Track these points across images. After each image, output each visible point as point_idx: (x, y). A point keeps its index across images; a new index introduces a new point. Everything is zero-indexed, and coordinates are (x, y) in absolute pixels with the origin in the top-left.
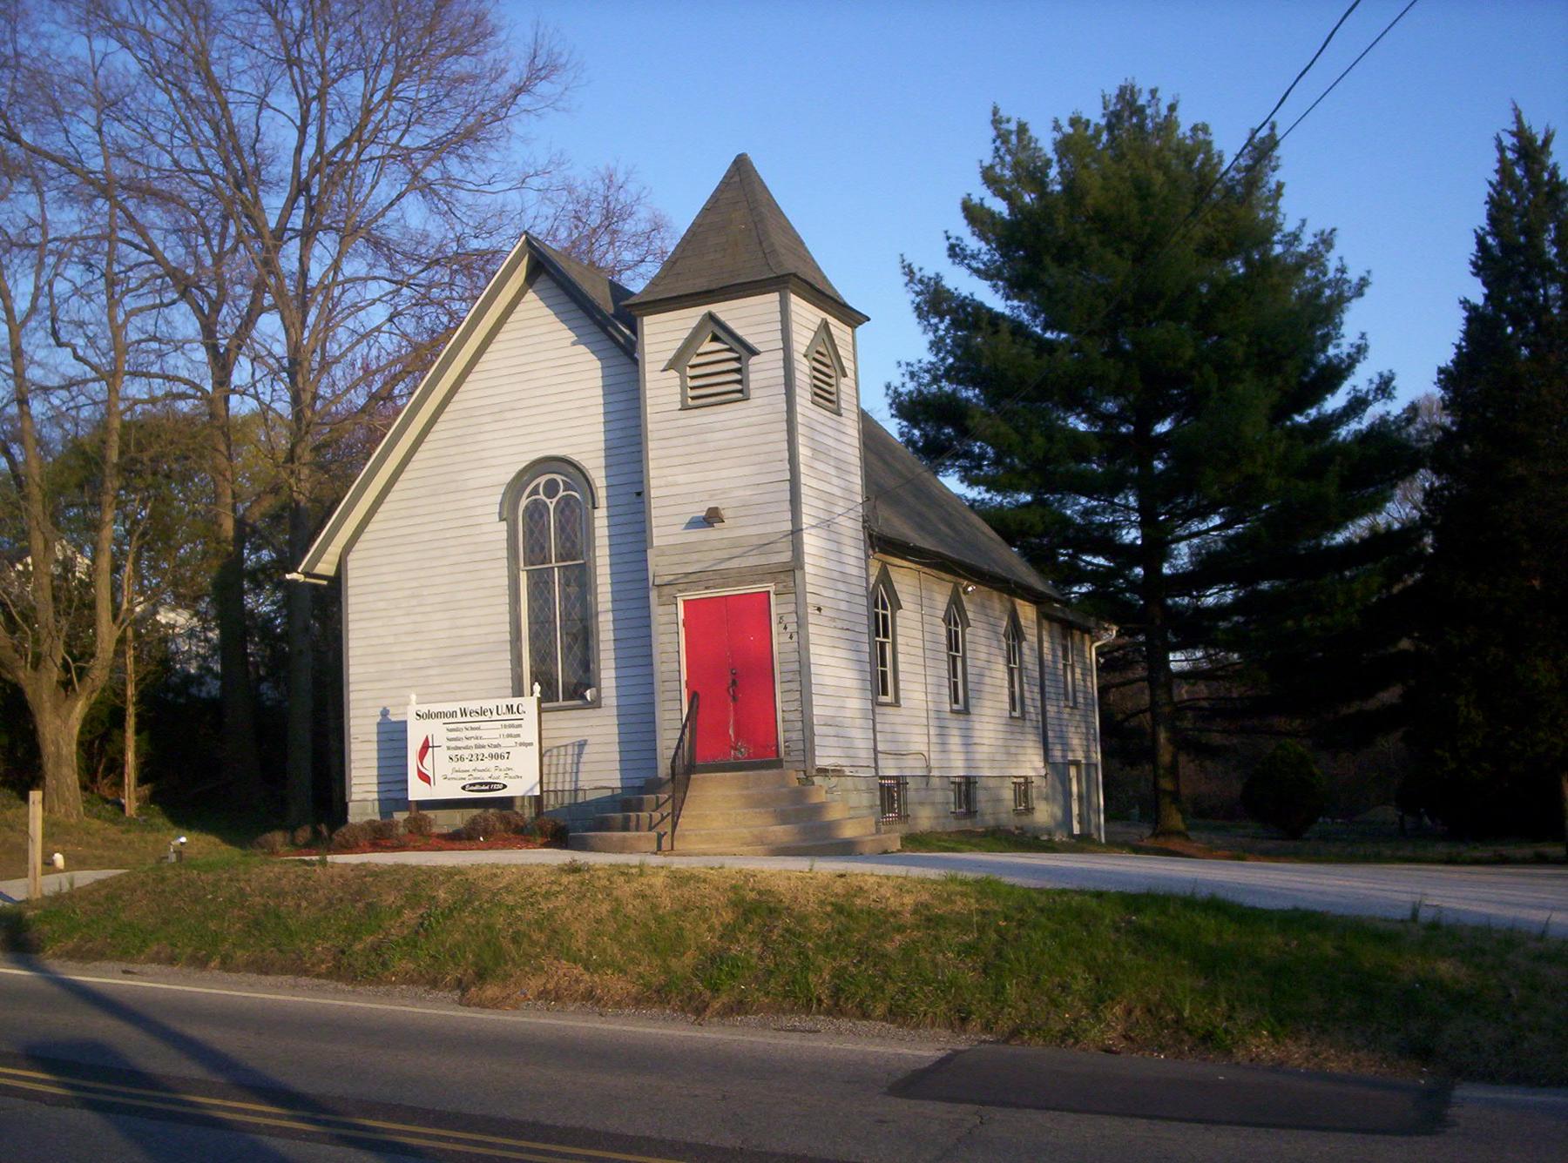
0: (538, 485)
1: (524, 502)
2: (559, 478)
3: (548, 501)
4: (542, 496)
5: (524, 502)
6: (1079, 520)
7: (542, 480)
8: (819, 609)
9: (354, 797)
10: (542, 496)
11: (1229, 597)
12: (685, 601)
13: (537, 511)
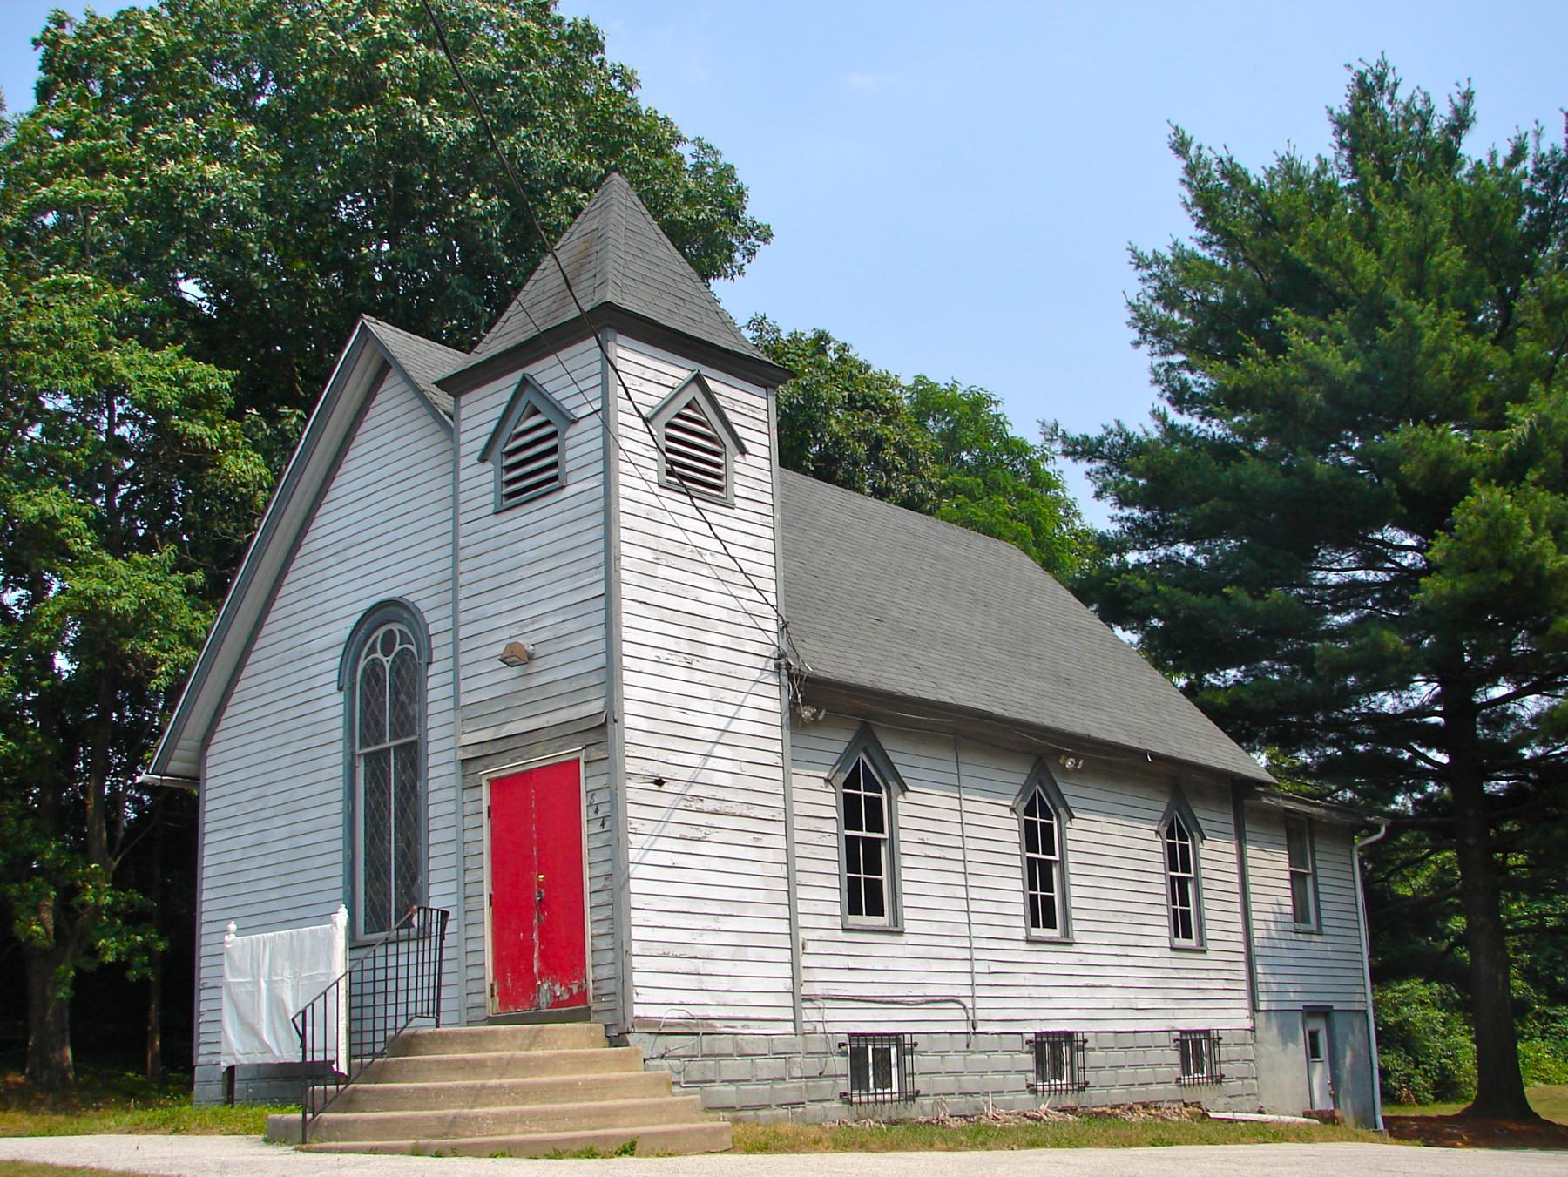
0: (375, 642)
1: (362, 664)
2: (395, 627)
3: (384, 659)
4: (379, 655)
5: (362, 664)
6: (1354, 181)
7: (380, 632)
8: (659, 782)
9: (201, 1060)
10: (379, 655)
11: (1516, 828)
12: (491, 781)
13: (374, 670)
